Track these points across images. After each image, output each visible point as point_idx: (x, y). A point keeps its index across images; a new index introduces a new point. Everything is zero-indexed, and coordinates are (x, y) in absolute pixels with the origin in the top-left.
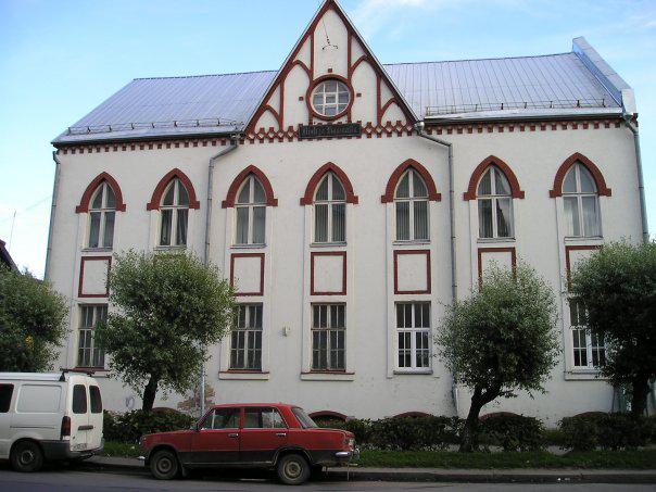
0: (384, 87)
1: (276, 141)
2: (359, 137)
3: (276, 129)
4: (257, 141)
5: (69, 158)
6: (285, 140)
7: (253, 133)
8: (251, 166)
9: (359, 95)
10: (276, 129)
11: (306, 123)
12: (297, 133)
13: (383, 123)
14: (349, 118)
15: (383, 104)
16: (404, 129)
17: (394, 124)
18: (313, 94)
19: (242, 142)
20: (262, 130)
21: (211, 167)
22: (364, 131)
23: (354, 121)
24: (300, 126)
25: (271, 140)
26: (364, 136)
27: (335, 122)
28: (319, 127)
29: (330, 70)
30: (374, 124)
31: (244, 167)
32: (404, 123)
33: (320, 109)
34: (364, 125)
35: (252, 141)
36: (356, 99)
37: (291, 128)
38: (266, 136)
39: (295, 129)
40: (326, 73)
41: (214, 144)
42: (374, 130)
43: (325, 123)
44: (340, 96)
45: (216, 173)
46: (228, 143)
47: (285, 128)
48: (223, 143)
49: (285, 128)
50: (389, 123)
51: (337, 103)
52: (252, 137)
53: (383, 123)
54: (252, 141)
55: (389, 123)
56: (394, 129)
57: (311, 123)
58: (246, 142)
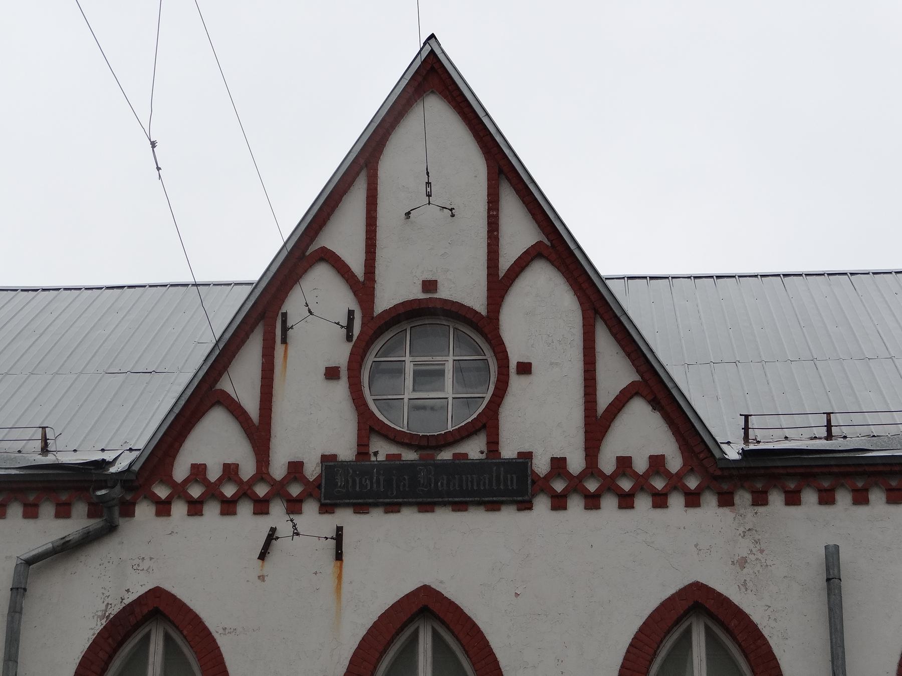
0: (605, 343)
1: (212, 510)
2: (526, 505)
3: (248, 470)
4: (179, 509)
5: (454, 400)
6: (179, 509)
7: (168, 480)
8: (426, 590)
9: (525, 369)
10: (248, 470)
11: (346, 450)
12: (317, 484)
13: (607, 464)
14: (493, 444)
15: (604, 400)
16: (676, 483)
17: (641, 465)
18: (370, 359)
19: (128, 511)
20: (198, 472)
21: (19, 591)
22: (541, 485)
23: (508, 451)
24: (328, 460)
25: (195, 508)
26: (542, 504)
27: (446, 455)
28: (393, 464)
29: (430, 286)
30: (576, 463)
31: (138, 586)
32: (675, 463)
33: (386, 404)
34: (541, 466)
35: (163, 508)
36: (516, 382)
37: (296, 468)
38: (212, 492)
39: (312, 470)
40: (415, 293)
41: (31, 512)
42: (576, 485)
43: (410, 456)
44: (459, 368)
45: (33, 608)
46: (80, 509)
47: (278, 470)
48: (63, 512)
49: (278, 470)
50: (624, 463)
51: (449, 389)
52: (162, 492)
53: (607, 464)
54: (163, 508)
55: (624, 463)
56: (642, 484)
57: (363, 450)
58: (144, 511)
